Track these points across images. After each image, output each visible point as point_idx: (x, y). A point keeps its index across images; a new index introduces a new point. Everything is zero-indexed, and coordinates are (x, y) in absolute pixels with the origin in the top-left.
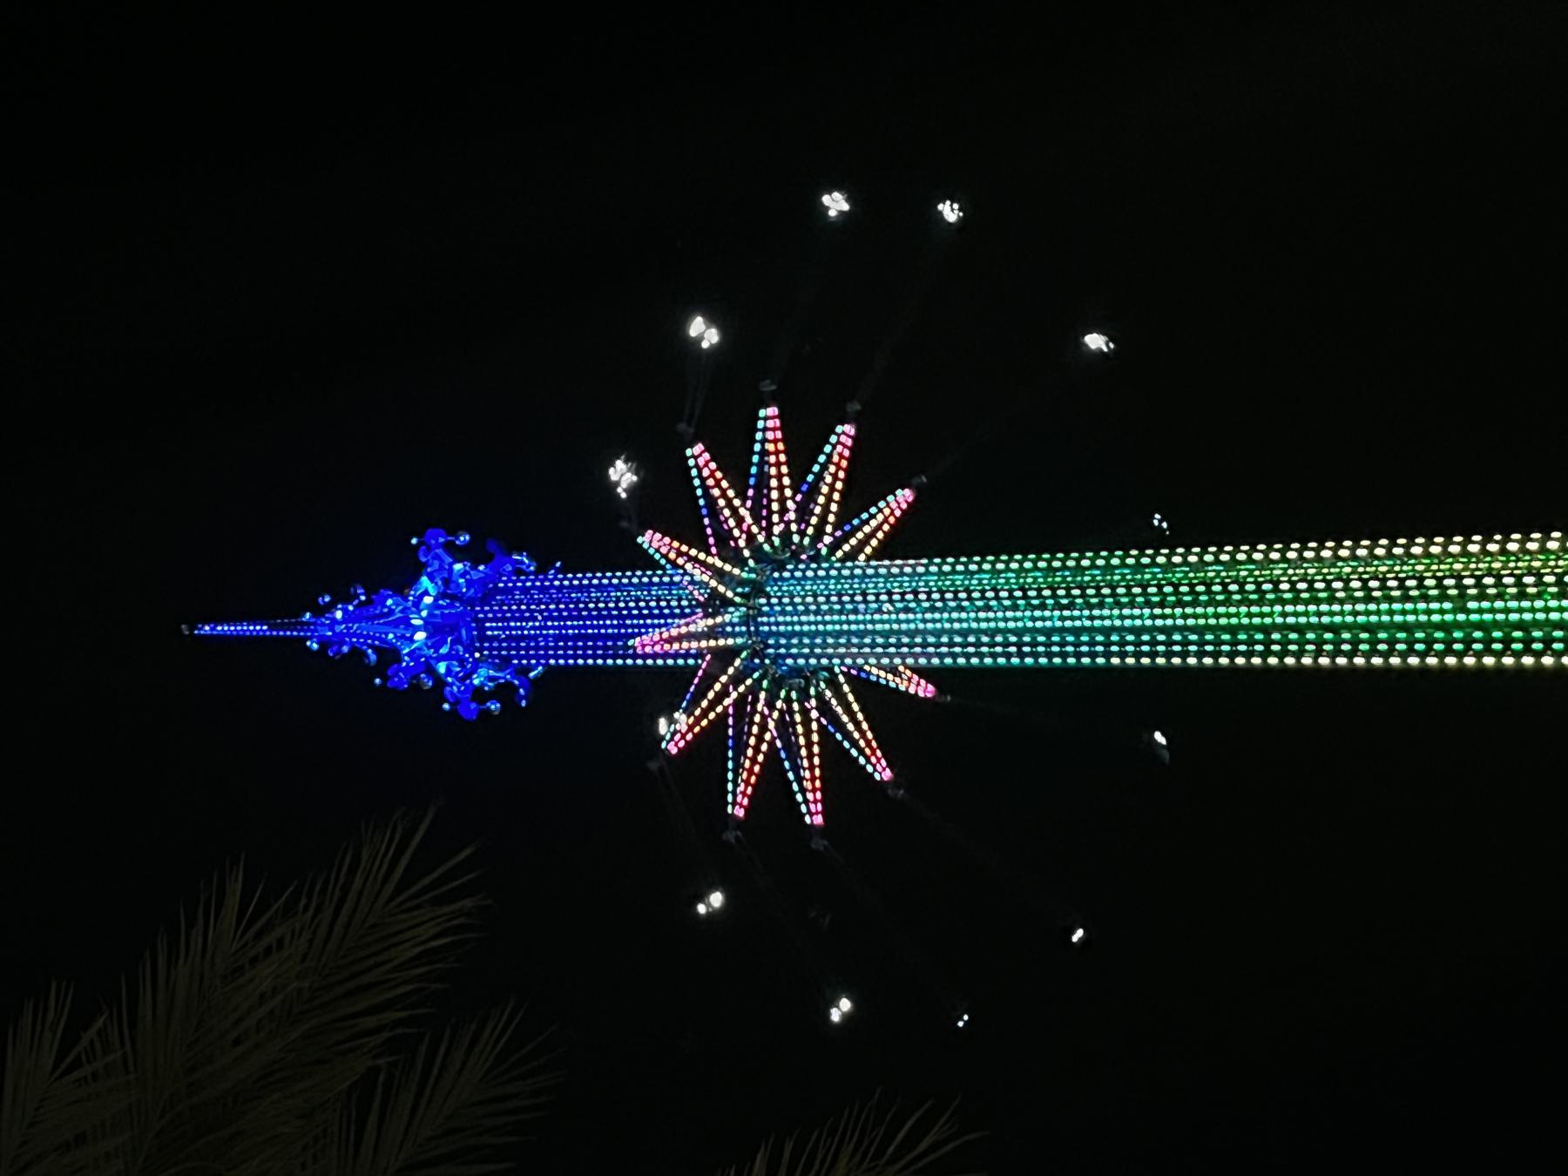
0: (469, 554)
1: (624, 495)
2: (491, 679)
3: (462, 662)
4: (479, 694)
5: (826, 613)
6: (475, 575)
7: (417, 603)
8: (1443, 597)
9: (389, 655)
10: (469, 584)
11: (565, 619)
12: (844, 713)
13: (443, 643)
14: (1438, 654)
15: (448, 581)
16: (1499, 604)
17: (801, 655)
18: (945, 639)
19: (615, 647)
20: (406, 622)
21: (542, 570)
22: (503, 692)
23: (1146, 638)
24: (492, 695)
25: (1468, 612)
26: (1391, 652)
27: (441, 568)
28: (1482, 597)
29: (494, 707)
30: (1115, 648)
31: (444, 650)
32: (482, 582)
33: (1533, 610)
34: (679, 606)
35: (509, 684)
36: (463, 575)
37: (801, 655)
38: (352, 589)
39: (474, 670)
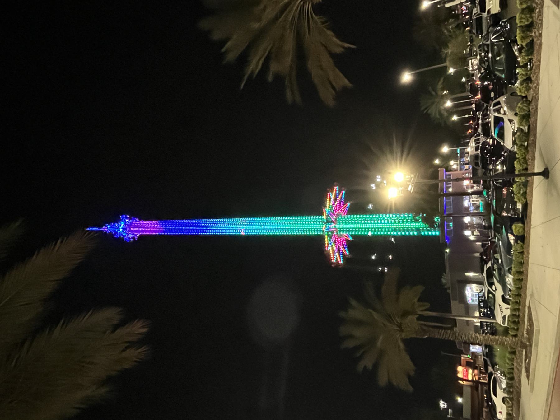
0: (130, 219)
1: (468, 134)
2: (131, 236)
3: (127, 234)
4: (130, 238)
5: (238, 226)
6: (129, 221)
7: (121, 225)
8: (259, 225)
9: (116, 233)
10: (129, 223)
11: (193, 227)
12: (92, 228)
13: (124, 231)
14: (256, 232)
15: (125, 222)
16: (265, 226)
17: (186, 233)
18: (226, 230)
19: (150, 231)
20: (119, 228)
21: (139, 221)
22: (133, 238)
23: (222, 230)
24: (131, 238)
25: (262, 227)
26: (248, 232)
27: (125, 220)
28: (263, 225)
29: (132, 240)
30: (222, 232)
31: (124, 232)
32: (131, 222)
33: (315, 226)
34: (210, 225)
35: (134, 237)
36: (128, 221)
37: (186, 233)
38: (505, 168)
39: (129, 235)
